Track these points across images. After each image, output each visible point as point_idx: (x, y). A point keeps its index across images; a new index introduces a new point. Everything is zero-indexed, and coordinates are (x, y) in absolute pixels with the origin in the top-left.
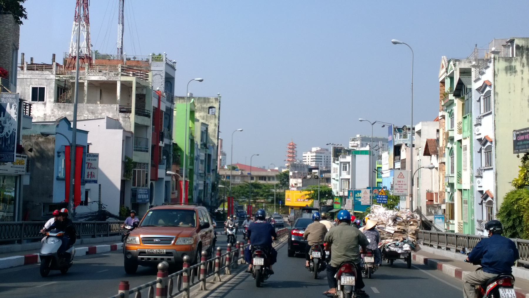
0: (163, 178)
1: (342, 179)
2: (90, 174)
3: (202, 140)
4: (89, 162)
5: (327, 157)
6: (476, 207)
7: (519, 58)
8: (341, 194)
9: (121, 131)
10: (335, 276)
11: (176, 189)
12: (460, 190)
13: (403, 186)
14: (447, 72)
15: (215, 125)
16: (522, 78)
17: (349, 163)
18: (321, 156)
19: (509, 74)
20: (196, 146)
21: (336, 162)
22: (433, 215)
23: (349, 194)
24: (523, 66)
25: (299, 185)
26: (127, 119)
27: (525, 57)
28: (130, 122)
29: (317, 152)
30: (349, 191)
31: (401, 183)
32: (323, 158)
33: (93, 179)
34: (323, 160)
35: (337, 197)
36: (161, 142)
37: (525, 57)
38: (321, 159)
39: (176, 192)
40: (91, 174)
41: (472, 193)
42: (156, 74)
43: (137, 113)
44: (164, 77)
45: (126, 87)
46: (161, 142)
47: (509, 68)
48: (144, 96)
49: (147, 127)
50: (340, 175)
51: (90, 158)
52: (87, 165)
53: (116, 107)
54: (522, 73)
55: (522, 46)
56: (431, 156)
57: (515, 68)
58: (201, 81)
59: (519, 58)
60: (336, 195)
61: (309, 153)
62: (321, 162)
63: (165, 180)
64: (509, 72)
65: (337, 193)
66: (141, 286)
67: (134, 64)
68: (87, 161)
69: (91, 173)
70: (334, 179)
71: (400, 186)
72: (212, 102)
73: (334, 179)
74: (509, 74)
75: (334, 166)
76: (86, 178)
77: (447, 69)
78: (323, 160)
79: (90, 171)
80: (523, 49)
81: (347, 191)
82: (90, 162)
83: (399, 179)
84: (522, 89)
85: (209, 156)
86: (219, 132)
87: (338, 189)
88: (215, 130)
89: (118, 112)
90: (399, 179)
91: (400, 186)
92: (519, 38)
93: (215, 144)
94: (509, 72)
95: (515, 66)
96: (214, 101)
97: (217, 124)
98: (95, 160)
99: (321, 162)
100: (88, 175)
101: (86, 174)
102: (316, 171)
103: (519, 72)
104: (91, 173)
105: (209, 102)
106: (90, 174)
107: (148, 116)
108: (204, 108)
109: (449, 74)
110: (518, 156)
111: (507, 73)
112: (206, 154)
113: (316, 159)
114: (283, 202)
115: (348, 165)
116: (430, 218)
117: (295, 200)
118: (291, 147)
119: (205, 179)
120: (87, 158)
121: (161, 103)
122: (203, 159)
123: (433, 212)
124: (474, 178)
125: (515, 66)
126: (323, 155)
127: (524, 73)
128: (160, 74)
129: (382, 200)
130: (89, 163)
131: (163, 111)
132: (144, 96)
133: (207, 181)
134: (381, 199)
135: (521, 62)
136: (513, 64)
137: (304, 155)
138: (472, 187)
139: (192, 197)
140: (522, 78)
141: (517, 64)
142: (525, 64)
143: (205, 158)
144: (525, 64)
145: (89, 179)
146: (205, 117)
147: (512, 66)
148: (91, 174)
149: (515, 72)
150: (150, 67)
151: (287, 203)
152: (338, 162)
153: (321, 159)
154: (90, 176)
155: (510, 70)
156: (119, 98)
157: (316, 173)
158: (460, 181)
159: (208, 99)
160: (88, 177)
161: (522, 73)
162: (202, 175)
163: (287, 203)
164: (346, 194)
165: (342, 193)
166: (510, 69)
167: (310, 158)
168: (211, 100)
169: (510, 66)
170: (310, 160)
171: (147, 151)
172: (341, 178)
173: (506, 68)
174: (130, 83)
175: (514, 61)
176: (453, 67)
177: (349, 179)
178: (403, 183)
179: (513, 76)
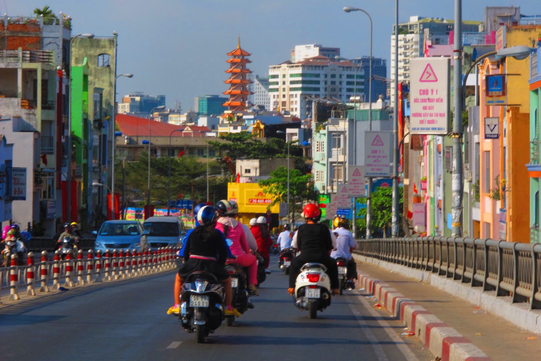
2: (17, 190)
3: (95, 114)
4: (15, 177)
5: (333, 76)
9: (31, 134)
10: (257, 261)
15: (111, 84)
17: (343, 133)
18: (318, 76)
20: (89, 126)
21: (322, 131)
25: (253, 174)
26: (31, 116)
28: (36, 120)
29: (307, 64)
32: (322, 79)
33: (21, 195)
34: (322, 86)
35: (323, 194)
38: (318, 82)
40: (19, 191)
42: (50, 43)
43: (43, 108)
44: (61, 47)
45: (29, 74)
46: (62, 137)
50: (330, 155)
51: (16, 173)
52: (13, 181)
53: (17, 101)
58: (131, 76)
61: (284, 66)
62: (317, 89)
65: (324, 188)
68: (13, 177)
69: (19, 189)
70: (318, 162)
72: (104, 47)
73: (318, 162)
75: (319, 139)
76: (13, 195)
78: (322, 86)
79: (17, 187)
82: (17, 177)
85: (105, 136)
86: (115, 94)
87: (325, 182)
88: (110, 94)
89: (20, 107)
93: (267, 267)
96: (107, 44)
97: (113, 83)
98: (23, 175)
99: (317, 89)
100: (15, 192)
101: (13, 191)
102: (296, 131)
104: (19, 189)
106: (17, 190)
112: (100, 136)
115: (342, 137)
117: (246, 201)
118: (238, 60)
119: (100, 176)
120: (13, 173)
126: (322, 72)
128: (55, 43)
130: (15, 179)
137: (272, 72)
139: (87, 206)
143: (100, 142)
145: (17, 195)
148: (19, 191)
150: (41, 33)
152: (325, 132)
154: (17, 193)
156: (20, 90)
157: (295, 134)
159: (98, 41)
160: (15, 194)
162: (96, 170)
167: (288, 79)
168: (102, 43)
170: (288, 85)
172: (330, 160)
174: (34, 71)
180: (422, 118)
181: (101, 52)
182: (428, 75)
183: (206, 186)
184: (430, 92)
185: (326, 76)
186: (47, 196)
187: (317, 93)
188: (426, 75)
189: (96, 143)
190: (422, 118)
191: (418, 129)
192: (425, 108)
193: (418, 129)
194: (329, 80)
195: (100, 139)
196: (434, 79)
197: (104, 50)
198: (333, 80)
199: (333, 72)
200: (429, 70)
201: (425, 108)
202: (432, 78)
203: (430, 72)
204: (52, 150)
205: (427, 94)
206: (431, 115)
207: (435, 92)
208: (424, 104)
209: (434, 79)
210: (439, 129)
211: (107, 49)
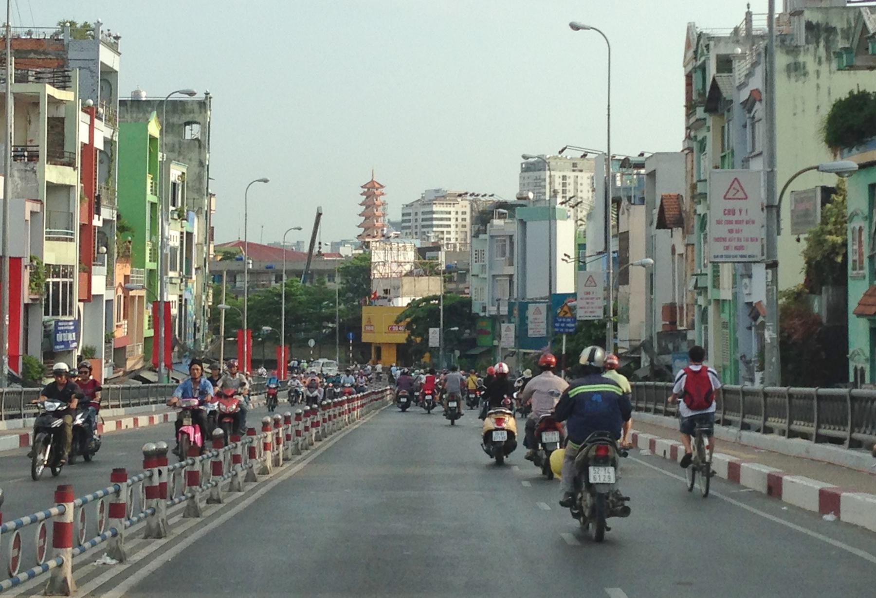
0: (102, 296)
1: (494, 276)
6: (741, 334)
7: (811, 47)
8: (492, 310)
11: (124, 318)
12: (717, 301)
13: (743, 227)
14: (695, 58)
16: (818, 86)
18: (450, 213)
19: (793, 79)
22: (669, 353)
23: (511, 311)
24: (820, 63)
26: (29, 174)
27: (822, 44)
28: (36, 181)
30: (511, 306)
31: (591, 296)
34: (453, 222)
36: (96, 216)
37: (822, 44)
38: (450, 219)
39: (124, 323)
41: (736, 306)
46: (96, 216)
47: (792, 66)
48: (62, 120)
49: (68, 188)
54: (818, 77)
55: (818, 25)
56: (671, 229)
57: (804, 67)
59: (811, 47)
60: (482, 314)
62: (449, 226)
63: (105, 299)
64: (793, 74)
66: (281, 446)
67: (29, 47)
71: (734, 227)
74: (793, 79)
77: (696, 52)
78: (453, 222)
80: (819, 30)
81: (506, 303)
83: (730, 204)
84: (818, 107)
90: (730, 204)
91: (734, 227)
92: (811, 9)
94: (793, 74)
95: (804, 63)
99: (449, 226)
103: (812, 75)
105: (184, 111)
107: (71, 164)
108: (173, 125)
109: (699, 63)
110: (798, 240)
111: (789, 76)
112: (182, 233)
113: (432, 219)
114: (358, 336)
116: (667, 358)
117: (385, 329)
121: (96, 131)
122: (177, 244)
123: (670, 346)
124: (738, 277)
125: (804, 63)
127: (821, 76)
129: (565, 327)
131: (96, 149)
132: (62, 120)
133: (186, 295)
134: (563, 325)
135: (815, 55)
136: (801, 59)
138: (735, 295)
140: (818, 86)
141: (807, 59)
142: (824, 59)
143: (182, 242)
144: (824, 59)
146: (177, 146)
147: (799, 63)
149: (805, 74)
151: (366, 338)
152: (486, 236)
153: (450, 219)
155: (796, 69)
158: (716, 285)
161: (818, 77)
162: (174, 281)
163: (366, 338)
164: (504, 310)
165: (495, 308)
166: (796, 70)
168: (189, 107)
169: (795, 63)
171: (71, 240)
173: (788, 66)
175: (802, 53)
176: (705, 52)
177: (511, 276)
178: (744, 217)
179: (800, 83)
180: (727, 244)
181: (188, 120)
182: (735, 191)
183: (281, 308)
184: (737, 212)
185: (457, 213)
186: (425, 217)
187: (449, 229)
188: (732, 192)
189: (175, 243)
190: (727, 244)
191: (722, 256)
192: (731, 231)
193: (722, 256)
194: (460, 216)
195: (182, 237)
196: (744, 196)
197: (191, 115)
198: (464, 216)
199: (464, 210)
200: (736, 185)
201: (731, 231)
202: (740, 195)
203: (738, 187)
204: (72, 234)
205: (734, 214)
206: (739, 240)
207: (743, 213)
208: (730, 227)
209: (744, 196)
210: (750, 256)
211: (196, 115)
